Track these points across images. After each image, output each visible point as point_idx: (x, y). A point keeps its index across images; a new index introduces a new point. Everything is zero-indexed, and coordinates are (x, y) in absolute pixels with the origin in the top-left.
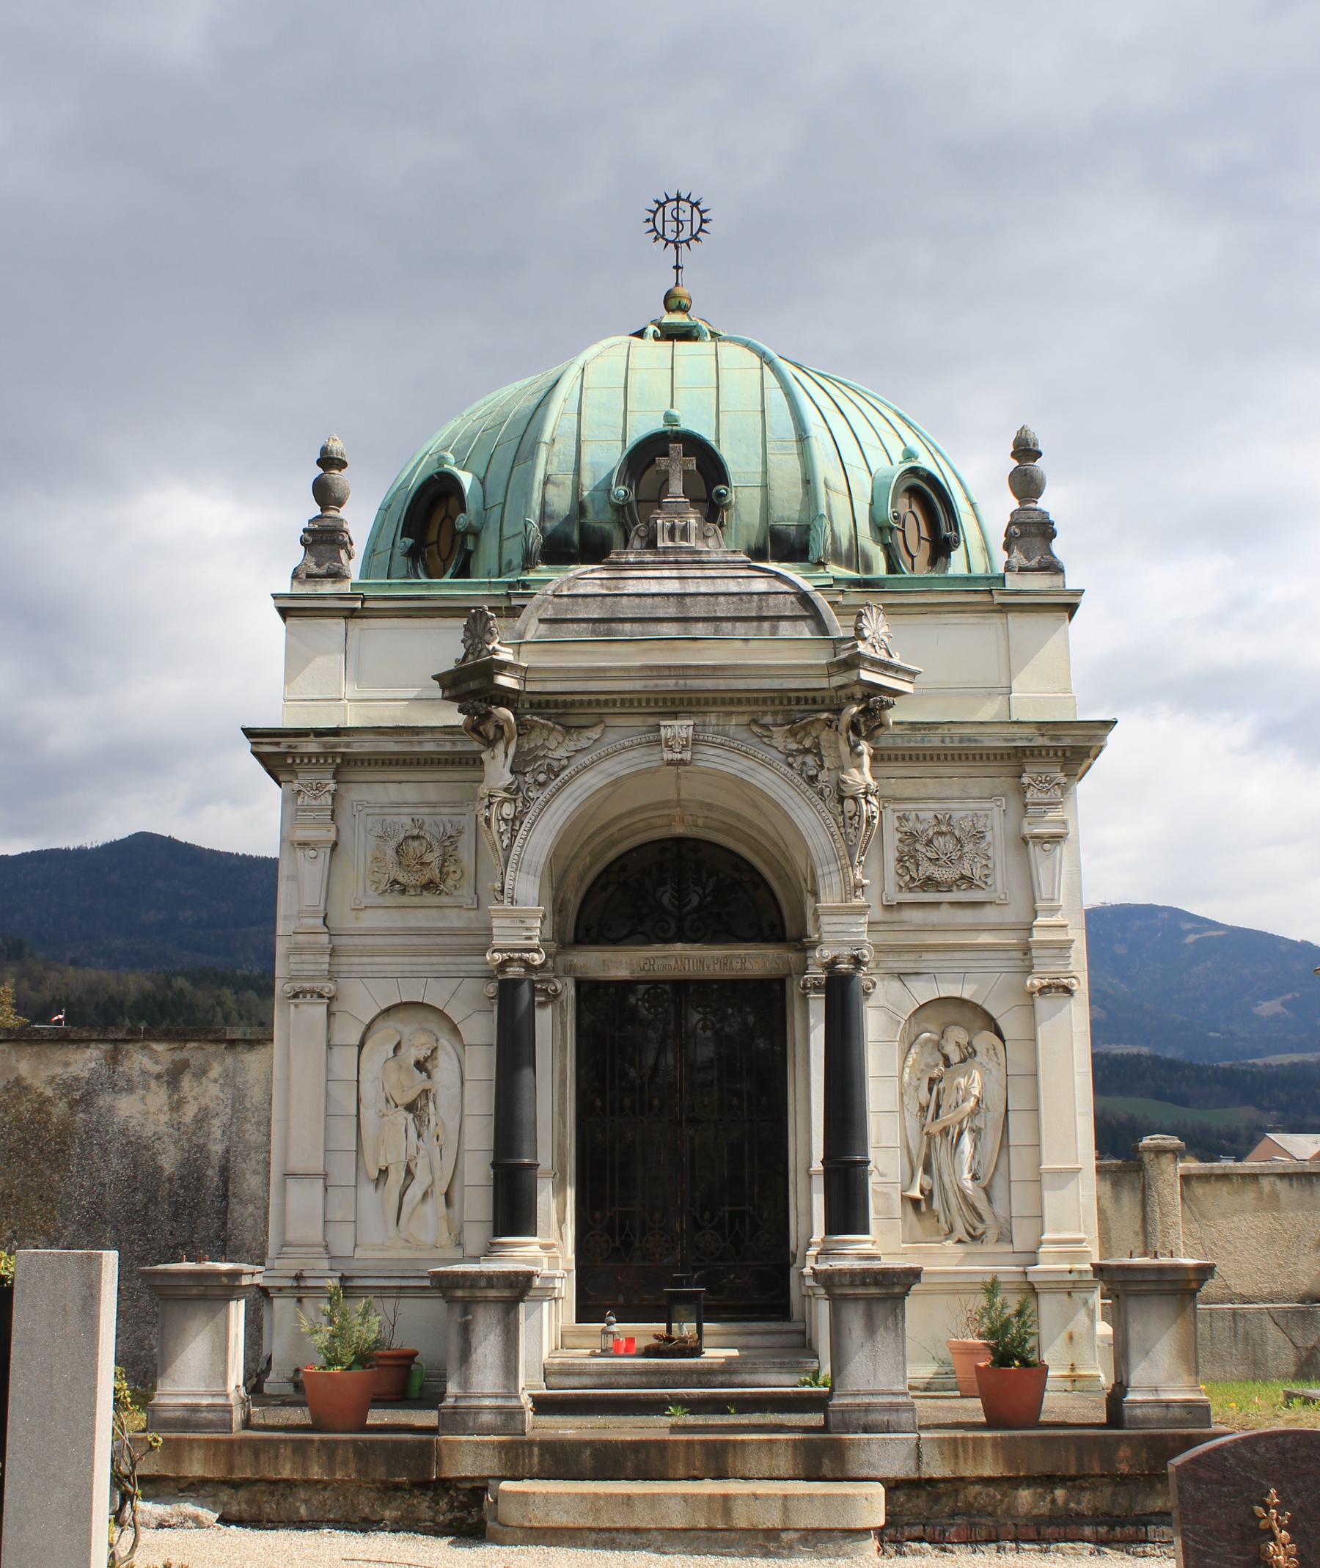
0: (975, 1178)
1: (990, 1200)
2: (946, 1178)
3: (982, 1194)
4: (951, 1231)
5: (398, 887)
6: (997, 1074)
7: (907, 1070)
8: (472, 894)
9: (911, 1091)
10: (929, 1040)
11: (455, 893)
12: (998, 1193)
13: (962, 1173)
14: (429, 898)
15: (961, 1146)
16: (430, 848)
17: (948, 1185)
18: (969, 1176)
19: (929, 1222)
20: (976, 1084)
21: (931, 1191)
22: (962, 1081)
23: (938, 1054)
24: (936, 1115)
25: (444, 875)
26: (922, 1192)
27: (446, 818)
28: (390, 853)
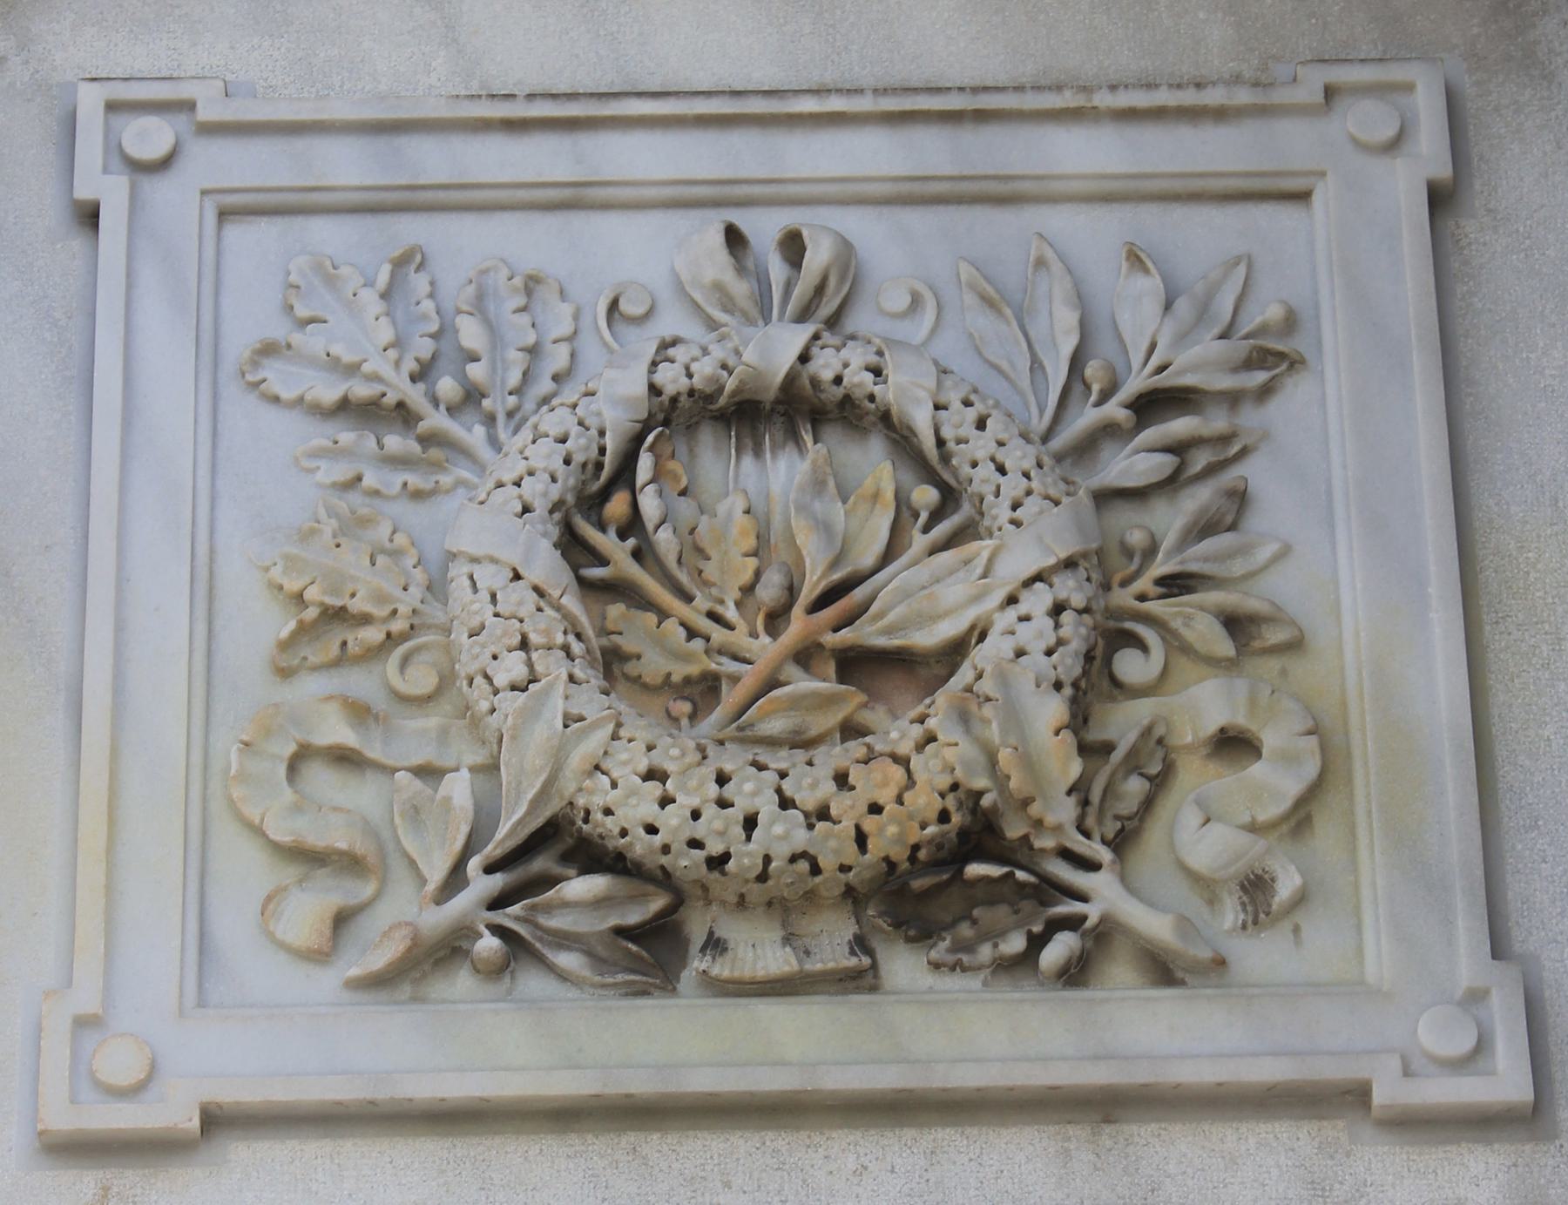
5: (581, 893)
8: (1466, 958)
11: (1261, 957)
14: (949, 1019)
16: (945, 504)
25: (1124, 792)
27: (1092, 235)
28: (491, 529)
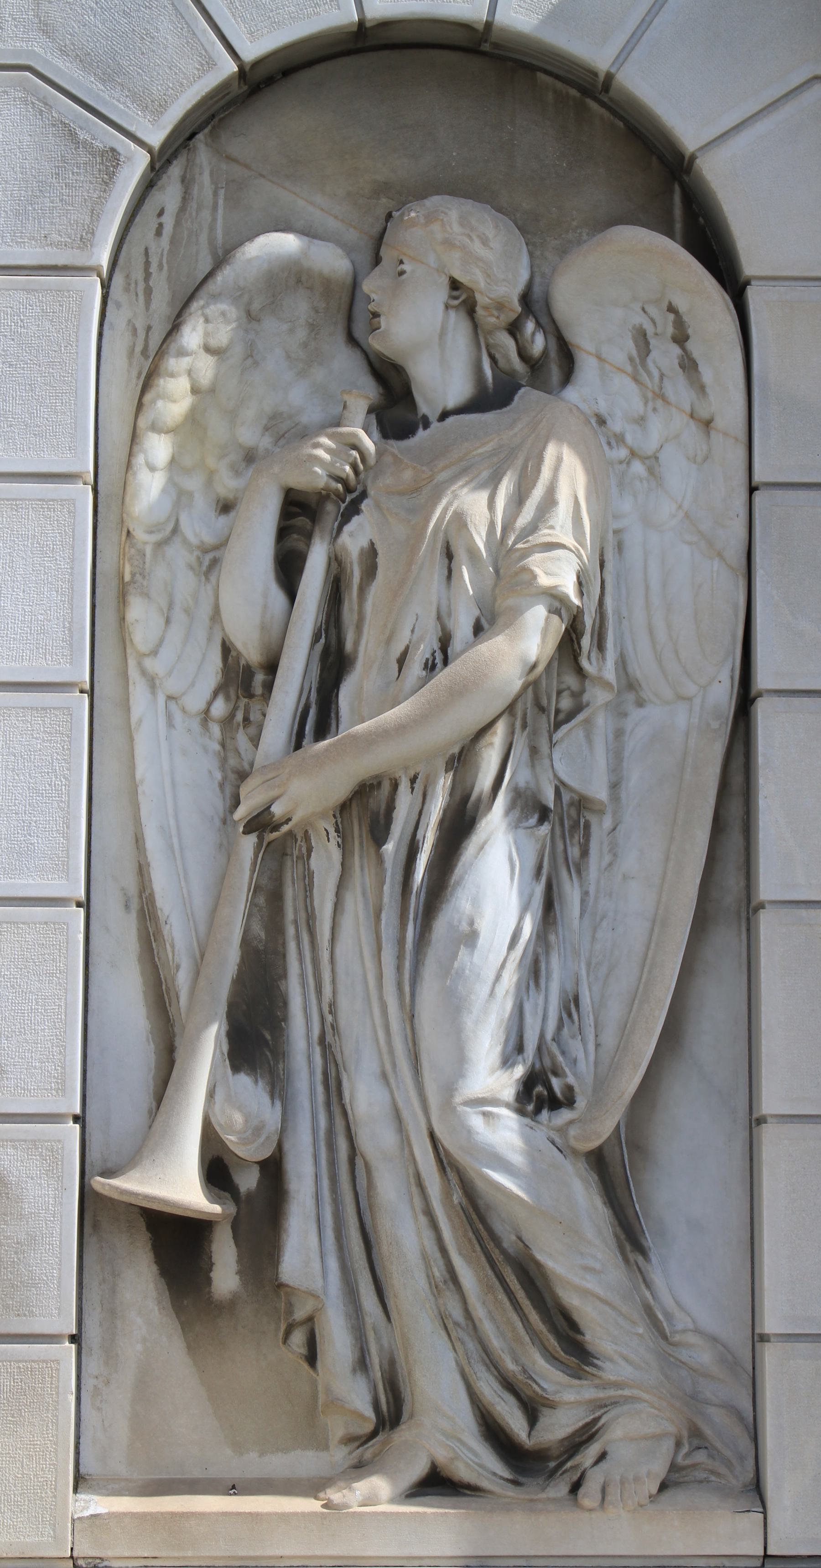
0: (539, 1095)
1: (631, 1236)
2: (366, 1097)
3: (584, 1197)
4: (391, 1413)
6: (693, 482)
7: (159, 449)
9: (176, 572)
10: (289, 278)
12: (684, 1186)
13: (460, 1061)
15: (460, 903)
17: (377, 1138)
18: (505, 1084)
19: (257, 1361)
20: (559, 526)
21: (273, 1169)
22: (477, 509)
23: (344, 364)
24: (320, 716)
26: (217, 1172)
